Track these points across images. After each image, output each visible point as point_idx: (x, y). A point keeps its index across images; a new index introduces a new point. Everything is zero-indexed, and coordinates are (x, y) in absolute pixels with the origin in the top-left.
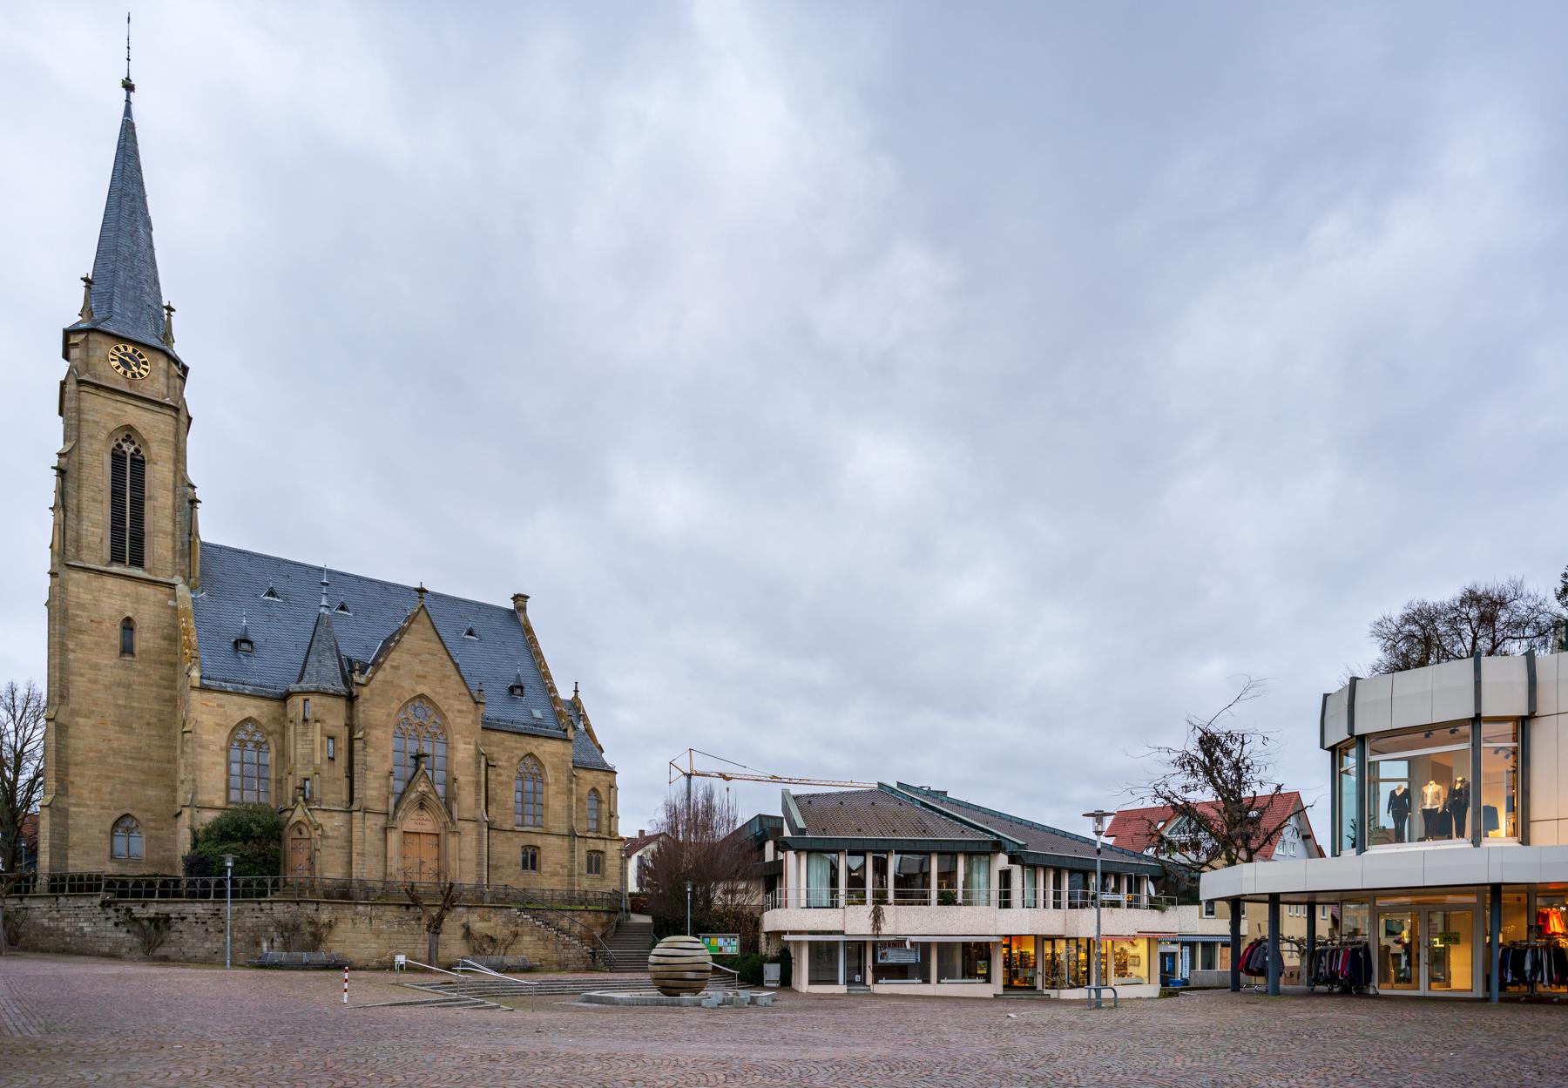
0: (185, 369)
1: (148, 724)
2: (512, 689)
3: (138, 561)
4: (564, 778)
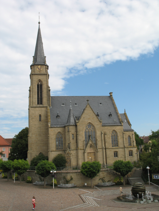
0: (48, 66)
1: (44, 134)
2: (109, 115)
3: (41, 104)
4: (122, 134)
